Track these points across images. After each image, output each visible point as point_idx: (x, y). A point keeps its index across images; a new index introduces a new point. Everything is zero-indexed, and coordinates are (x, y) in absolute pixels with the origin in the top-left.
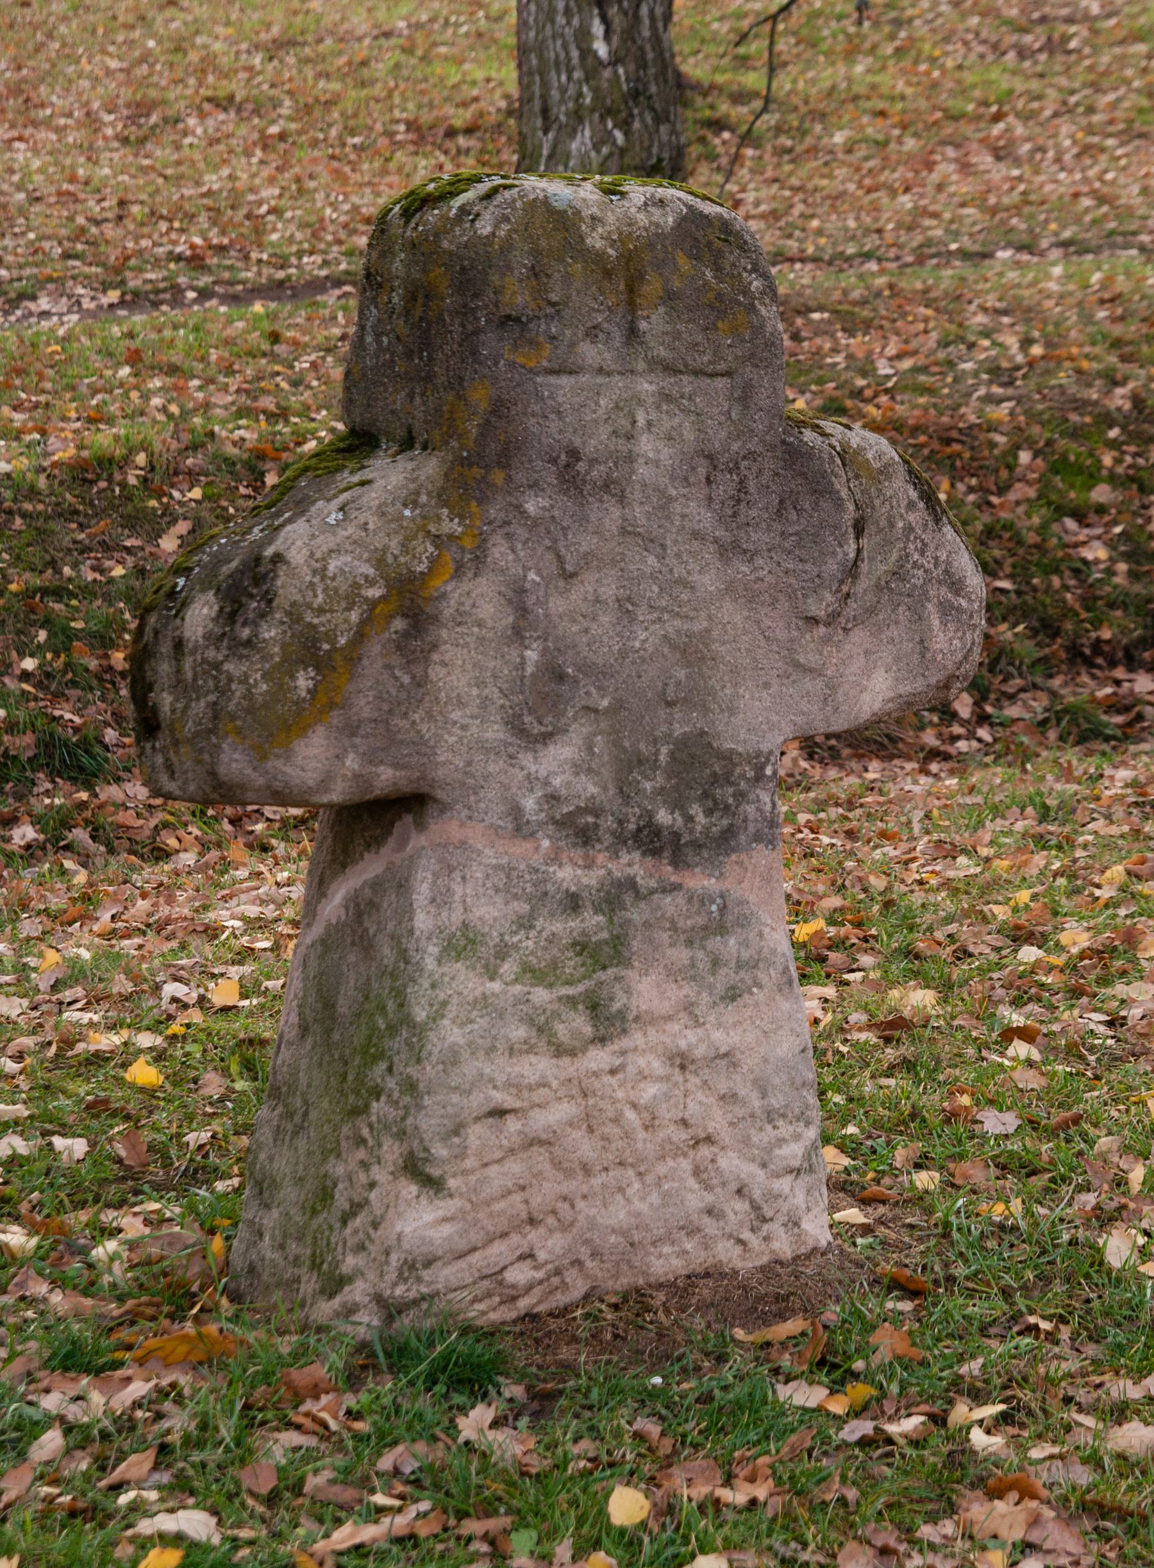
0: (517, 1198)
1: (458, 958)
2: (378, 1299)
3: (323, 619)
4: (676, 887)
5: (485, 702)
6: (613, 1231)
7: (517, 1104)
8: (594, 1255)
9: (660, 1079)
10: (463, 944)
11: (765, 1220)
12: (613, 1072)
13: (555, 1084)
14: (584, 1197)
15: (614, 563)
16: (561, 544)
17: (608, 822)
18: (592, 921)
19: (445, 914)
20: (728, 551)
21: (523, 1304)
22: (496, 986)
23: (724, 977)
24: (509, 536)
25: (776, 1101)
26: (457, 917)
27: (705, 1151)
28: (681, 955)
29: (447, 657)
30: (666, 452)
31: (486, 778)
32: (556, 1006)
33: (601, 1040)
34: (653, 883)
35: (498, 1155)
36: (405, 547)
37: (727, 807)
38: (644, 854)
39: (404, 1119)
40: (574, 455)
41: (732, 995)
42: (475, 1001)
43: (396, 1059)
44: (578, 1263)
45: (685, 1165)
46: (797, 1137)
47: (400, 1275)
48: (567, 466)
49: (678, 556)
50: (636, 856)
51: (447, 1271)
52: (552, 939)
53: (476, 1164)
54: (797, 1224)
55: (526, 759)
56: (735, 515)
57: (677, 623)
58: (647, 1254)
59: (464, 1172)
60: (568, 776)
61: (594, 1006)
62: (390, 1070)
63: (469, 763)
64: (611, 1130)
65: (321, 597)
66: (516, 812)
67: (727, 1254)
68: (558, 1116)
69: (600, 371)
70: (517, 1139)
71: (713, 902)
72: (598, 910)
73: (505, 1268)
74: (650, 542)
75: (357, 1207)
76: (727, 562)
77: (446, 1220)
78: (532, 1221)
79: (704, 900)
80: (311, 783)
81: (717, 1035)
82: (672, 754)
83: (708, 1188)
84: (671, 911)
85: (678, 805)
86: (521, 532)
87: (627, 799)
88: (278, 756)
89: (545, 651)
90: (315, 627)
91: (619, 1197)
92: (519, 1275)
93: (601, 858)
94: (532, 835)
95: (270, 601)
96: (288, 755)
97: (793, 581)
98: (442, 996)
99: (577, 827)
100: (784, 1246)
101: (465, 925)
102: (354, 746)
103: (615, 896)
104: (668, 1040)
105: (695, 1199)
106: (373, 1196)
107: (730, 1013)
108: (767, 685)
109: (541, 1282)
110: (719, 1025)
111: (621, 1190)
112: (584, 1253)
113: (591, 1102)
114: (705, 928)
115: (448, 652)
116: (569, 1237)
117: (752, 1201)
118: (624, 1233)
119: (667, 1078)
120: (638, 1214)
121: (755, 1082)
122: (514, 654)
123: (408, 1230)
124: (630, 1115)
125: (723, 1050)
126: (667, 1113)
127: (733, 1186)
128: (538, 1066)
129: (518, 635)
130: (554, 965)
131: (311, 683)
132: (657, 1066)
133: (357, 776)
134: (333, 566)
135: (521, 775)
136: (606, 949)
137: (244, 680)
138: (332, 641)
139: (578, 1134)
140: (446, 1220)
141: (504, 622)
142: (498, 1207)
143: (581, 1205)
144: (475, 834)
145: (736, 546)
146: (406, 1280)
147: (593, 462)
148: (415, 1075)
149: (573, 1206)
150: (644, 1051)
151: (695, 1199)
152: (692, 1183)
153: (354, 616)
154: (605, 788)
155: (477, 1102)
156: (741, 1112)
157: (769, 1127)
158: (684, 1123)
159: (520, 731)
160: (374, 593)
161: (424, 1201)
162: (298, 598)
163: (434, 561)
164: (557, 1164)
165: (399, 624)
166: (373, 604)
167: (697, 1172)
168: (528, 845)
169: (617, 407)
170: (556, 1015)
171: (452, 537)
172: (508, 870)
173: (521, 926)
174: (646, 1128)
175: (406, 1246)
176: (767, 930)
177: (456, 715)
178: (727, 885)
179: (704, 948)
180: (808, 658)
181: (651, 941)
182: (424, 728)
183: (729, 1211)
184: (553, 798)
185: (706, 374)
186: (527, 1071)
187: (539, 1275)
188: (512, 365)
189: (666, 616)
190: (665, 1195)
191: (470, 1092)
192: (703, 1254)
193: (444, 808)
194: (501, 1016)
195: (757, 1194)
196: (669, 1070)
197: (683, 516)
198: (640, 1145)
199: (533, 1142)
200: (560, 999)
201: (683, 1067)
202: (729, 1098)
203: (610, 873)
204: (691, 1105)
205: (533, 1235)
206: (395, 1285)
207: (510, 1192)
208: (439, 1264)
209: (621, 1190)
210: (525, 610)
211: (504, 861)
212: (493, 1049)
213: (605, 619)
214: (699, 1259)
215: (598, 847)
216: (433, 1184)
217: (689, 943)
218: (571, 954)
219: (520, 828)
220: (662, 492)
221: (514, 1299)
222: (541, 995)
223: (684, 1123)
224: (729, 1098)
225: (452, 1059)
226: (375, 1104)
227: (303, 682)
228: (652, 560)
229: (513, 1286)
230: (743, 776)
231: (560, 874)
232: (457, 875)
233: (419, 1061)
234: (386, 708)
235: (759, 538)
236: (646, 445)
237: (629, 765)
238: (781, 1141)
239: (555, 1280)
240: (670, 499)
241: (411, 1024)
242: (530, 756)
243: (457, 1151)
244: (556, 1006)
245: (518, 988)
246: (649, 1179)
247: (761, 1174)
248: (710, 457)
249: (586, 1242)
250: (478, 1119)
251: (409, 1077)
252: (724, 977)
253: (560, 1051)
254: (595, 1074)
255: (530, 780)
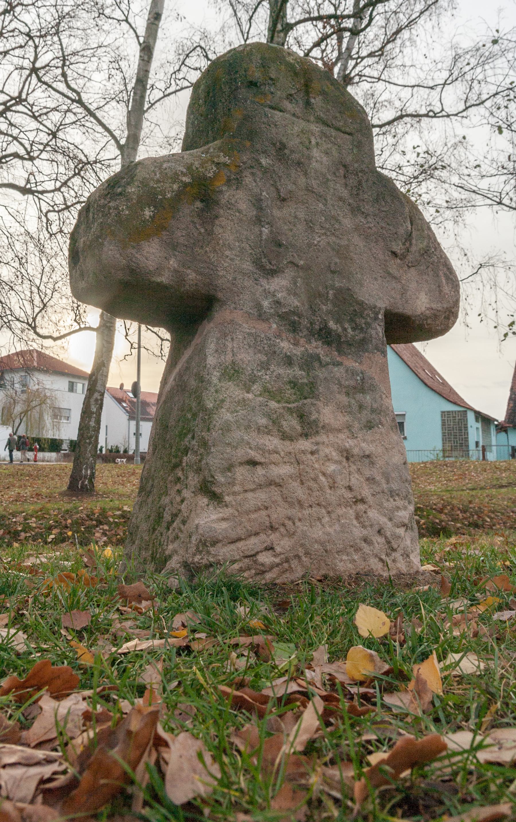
0: (264, 513)
1: (230, 379)
2: (186, 565)
3: (159, 185)
4: (339, 364)
5: (242, 250)
6: (316, 541)
7: (263, 460)
8: (307, 554)
9: (336, 462)
10: (232, 372)
11: (394, 550)
12: (312, 453)
13: (282, 454)
14: (300, 520)
15: (303, 203)
16: (278, 184)
17: (305, 322)
18: (297, 372)
19: (223, 357)
20: (355, 210)
21: (269, 576)
22: (250, 396)
23: (365, 415)
24: (253, 174)
25: (395, 486)
26: (229, 357)
27: (361, 507)
28: (343, 399)
29: (223, 224)
30: (325, 159)
31: (243, 288)
32: (282, 411)
33: (306, 435)
34: (328, 359)
35: (252, 487)
36: (202, 165)
37: (362, 328)
38: (323, 343)
39: (200, 461)
40: (283, 146)
41: (369, 426)
42: (239, 402)
43: (196, 429)
44: (297, 557)
45: (351, 512)
46: (405, 508)
47: (198, 548)
48: (280, 149)
49: (333, 206)
50: (320, 343)
51: (225, 550)
52: (278, 376)
53: (241, 489)
54: (408, 556)
55: (263, 282)
56: (358, 194)
57: (334, 238)
58: (335, 558)
59: (234, 494)
60: (284, 294)
61: (302, 417)
62: (193, 438)
63: (235, 279)
64: (312, 484)
65: (158, 175)
66: (259, 306)
67: (375, 565)
68: (284, 471)
69: (294, 115)
70: (263, 479)
71: (358, 375)
72: (301, 368)
73: (257, 553)
74: (320, 197)
75: (175, 516)
76: (355, 215)
77: (223, 519)
78: (272, 528)
79: (353, 373)
80: (151, 268)
81: (363, 445)
82: (335, 295)
83: (364, 527)
84: (338, 375)
85: (338, 321)
86: (259, 174)
87: (314, 312)
88: (134, 247)
89: (271, 232)
90: (155, 188)
91: (318, 523)
92: (265, 558)
93: (302, 341)
94: (268, 320)
95: (133, 178)
96: (139, 248)
97: (384, 232)
98: (221, 397)
99: (291, 322)
100: (402, 566)
101: (233, 363)
102: (174, 255)
103: (310, 362)
104: (339, 442)
105: (358, 532)
106: (183, 506)
107: (369, 435)
108: (376, 279)
109: (278, 565)
110: (364, 440)
111: (319, 519)
112: (301, 552)
113: (301, 467)
114: (355, 388)
115: (223, 221)
116: (293, 541)
117: (386, 538)
118: (322, 544)
119: (340, 462)
120: (329, 534)
121: (383, 474)
122: (257, 229)
123: (202, 522)
124: (322, 478)
125: (367, 453)
126: (341, 481)
127: (376, 528)
128: (273, 442)
129: (258, 221)
130: (280, 391)
131: (152, 214)
132: (335, 455)
133: (176, 271)
134: (165, 165)
135: (261, 289)
136: (306, 388)
137: (116, 208)
138: (164, 195)
139: (296, 484)
140: (223, 519)
141: (251, 214)
142: (253, 516)
143: (298, 524)
144: (238, 316)
145: (358, 209)
146: (201, 552)
147: (292, 152)
148: (207, 438)
149: (294, 524)
150: (328, 445)
151: (358, 532)
152: (355, 522)
153: (175, 187)
154: (303, 304)
155: (241, 453)
156: (378, 489)
157: (391, 500)
158: (350, 488)
159: (261, 267)
160: (186, 179)
161: (211, 508)
162: (147, 176)
163: (216, 175)
164: (285, 499)
165: (198, 204)
166: (186, 185)
167: (357, 517)
168: (265, 325)
169: (302, 131)
170: (282, 415)
171: (225, 165)
172: (255, 336)
173: (263, 368)
174: (331, 488)
175: (200, 531)
176: (384, 396)
177: (228, 253)
178: (364, 367)
179: (354, 398)
180: (393, 271)
181: (329, 388)
182: (212, 255)
183: (375, 541)
184: (278, 303)
185: (341, 131)
186: (267, 443)
187: (277, 560)
188: (253, 102)
189: (328, 233)
190: (342, 526)
191: (236, 448)
192: (363, 563)
193: (223, 303)
194: (253, 410)
195: (388, 534)
196: (341, 458)
197: (335, 189)
198: (328, 496)
199: (271, 483)
200: (284, 408)
201: (347, 459)
202: (370, 480)
203: (307, 350)
204: (353, 479)
205: (274, 537)
206: (194, 555)
207: (260, 509)
208: (220, 545)
209: (319, 519)
210: (261, 209)
211: (254, 331)
212: (249, 427)
213: (299, 227)
214: (362, 566)
215: (301, 334)
216: (216, 498)
217: (348, 394)
218: (288, 387)
219: (261, 316)
220: (324, 176)
221: (263, 572)
222: (273, 404)
223: (350, 488)
224: (370, 480)
225: (227, 429)
226: (185, 458)
227: (147, 213)
228: (320, 205)
229: (262, 565)
230: (368, 315)
231: (282, 345)
232: (229, 338)
233: (209, 430)
234: (192, 241)
235: (368, 208)
236: (316, 153)
237: (315, 297)
238: (398, 508)
239: (286, 565)
240: (328, 180)
241: (205, 409)
242: (265, 281)
243: (230, 480)
244: (282, 411)
245: (261, 399)
246: (333, 516)
247: (389, 524)
248: (345, 166)
249: (302, 545)
250: (241, 464)
251: (203, 438)
252: (365, 415)
253: (285, 437)
254: (304, 452)
255: (267, 293)
